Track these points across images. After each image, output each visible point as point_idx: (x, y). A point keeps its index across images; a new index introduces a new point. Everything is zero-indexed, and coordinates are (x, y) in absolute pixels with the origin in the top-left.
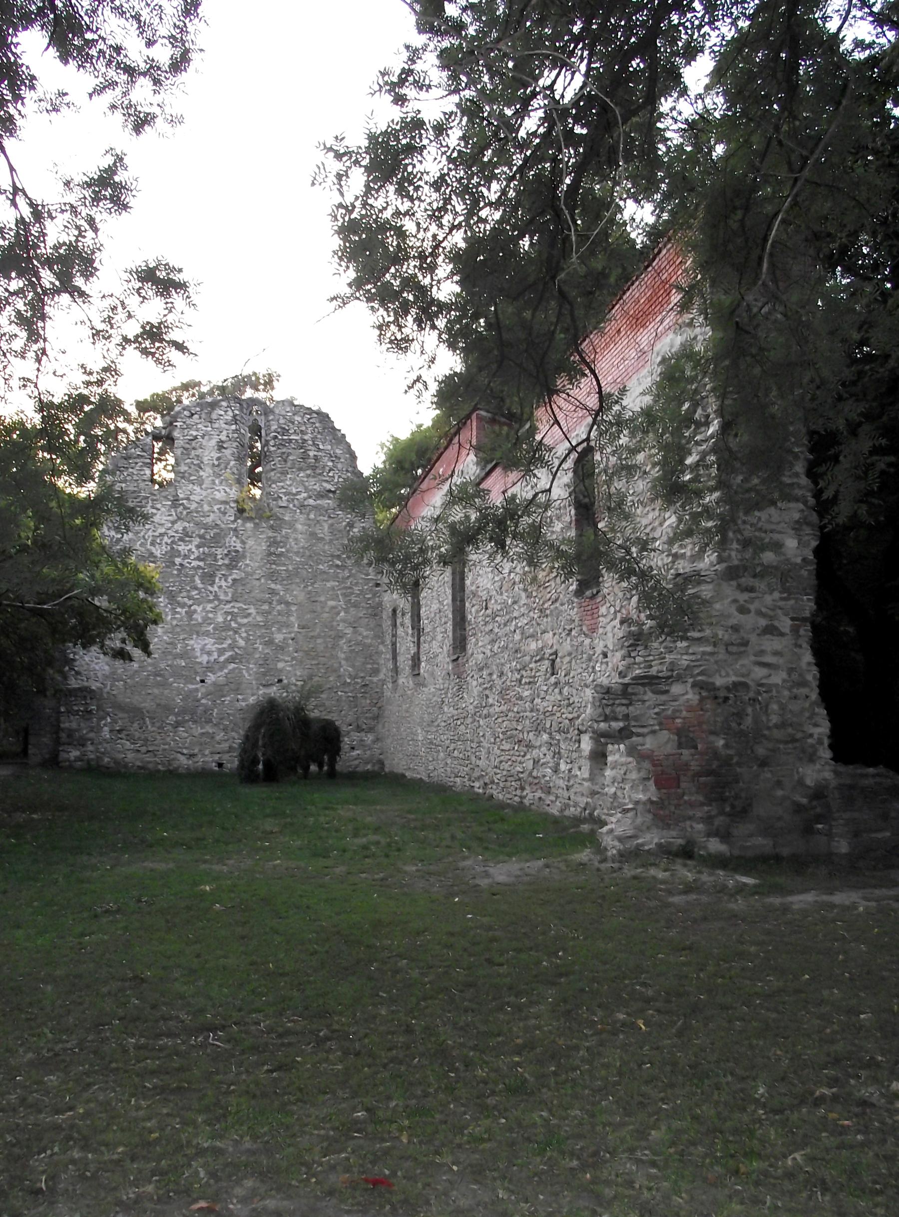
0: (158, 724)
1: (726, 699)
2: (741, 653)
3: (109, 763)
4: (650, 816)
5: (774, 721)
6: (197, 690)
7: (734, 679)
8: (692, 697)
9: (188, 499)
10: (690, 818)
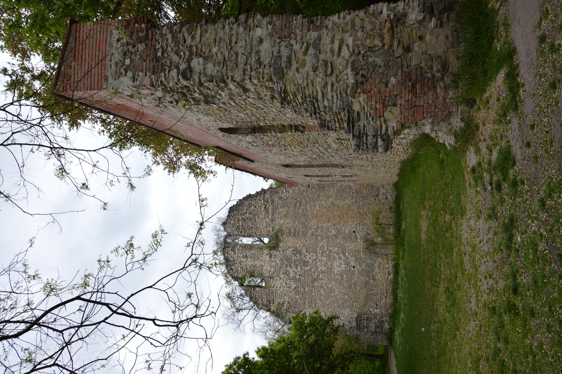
0: (374, 288)
1: (363, 76)
2: (332, 65)
3: (391, 310)
4: (442, 123)
5: (378, 42)
6: (358, 270)
7: (349, 70)
8: (362, 98)
9: (269, 272)
10: (445, 99)
